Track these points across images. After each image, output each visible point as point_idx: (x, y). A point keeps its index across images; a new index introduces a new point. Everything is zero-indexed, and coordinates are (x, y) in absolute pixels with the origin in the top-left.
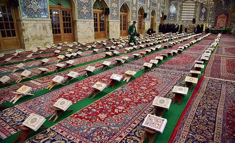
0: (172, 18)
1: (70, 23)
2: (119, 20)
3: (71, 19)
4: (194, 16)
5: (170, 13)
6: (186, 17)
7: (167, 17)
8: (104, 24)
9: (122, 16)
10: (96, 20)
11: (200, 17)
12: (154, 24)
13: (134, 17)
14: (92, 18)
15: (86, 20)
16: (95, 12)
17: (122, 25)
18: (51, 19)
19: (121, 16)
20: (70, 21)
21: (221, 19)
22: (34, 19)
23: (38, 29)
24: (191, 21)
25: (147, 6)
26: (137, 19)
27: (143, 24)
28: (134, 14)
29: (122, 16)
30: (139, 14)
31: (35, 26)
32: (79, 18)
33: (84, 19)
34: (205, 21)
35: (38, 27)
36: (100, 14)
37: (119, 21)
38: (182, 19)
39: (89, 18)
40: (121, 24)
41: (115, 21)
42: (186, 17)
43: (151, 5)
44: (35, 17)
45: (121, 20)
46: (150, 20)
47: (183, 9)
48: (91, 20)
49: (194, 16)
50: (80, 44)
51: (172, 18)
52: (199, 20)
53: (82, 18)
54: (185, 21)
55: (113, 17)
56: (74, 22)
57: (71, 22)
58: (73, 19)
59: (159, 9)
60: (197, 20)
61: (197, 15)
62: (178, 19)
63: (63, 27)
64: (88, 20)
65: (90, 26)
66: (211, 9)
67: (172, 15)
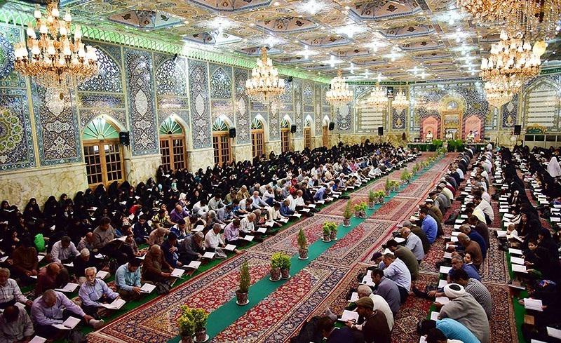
0: (344, 126)
1: (182, 156)
3: (184, 150)
8: (228, 150)
9: (255, 136)
10: (216, 146)
11: (395, 121)
15: (147, 156)
16: (86, 146)
17: (256, 148)
18: (86, 162)
19: (253, 135)
21: (429, 125)
22: (143, 156)
23: (147, 168)
24: (376, 129)
25: (296, 113)
27: (291, 142)
28: (202, 134)
29: (255, 136)
31: (143, 165)
32: (194, 148)
34: (404, 128)
35: (147, 166)
36: (222, 137)
37: (251, 143)
38: (363, 127)
40: (254, 147)
44: (144, 154)
45: (253, 142)
47: (530, 115)
52: (393, 128)
53: (198, 147)
54: (369, 129)
55: (242, 140)
56: (188, 153)
62: (355, 127)
63: (103, 176)
66: (496, 117)
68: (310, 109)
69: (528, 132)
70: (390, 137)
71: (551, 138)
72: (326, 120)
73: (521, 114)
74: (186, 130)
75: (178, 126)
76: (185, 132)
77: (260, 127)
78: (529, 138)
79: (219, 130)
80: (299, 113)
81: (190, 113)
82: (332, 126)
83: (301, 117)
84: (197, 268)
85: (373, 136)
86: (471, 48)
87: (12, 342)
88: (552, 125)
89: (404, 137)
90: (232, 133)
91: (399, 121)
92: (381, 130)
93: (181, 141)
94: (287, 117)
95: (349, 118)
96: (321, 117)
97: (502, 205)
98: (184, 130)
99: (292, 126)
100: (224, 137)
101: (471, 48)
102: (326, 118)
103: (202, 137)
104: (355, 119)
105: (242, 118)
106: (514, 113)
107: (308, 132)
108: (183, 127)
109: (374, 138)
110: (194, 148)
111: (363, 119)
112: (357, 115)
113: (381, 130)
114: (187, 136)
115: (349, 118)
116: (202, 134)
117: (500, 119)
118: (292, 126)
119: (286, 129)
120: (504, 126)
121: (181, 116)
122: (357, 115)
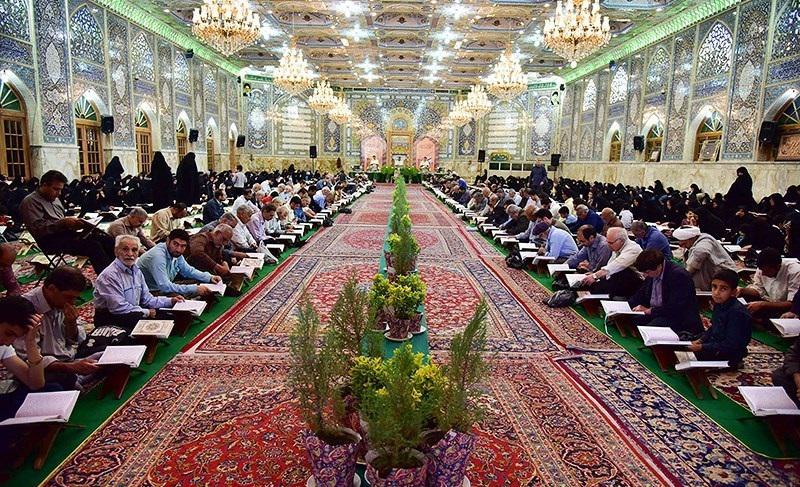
0: (258, 142)
1: (21, 152)
2: (73, 142)
4: (311, 139)
5: (253, 131)
6: (294, 141)
7: (247, 139)
8: (97, 154)
11: (327, 142)
12: (216, 157)
13: (124, 135)
14: (73, 140)
15: (61, 145)
19: (79, 130)
20: (21, 146)
26: (135, 141)
30: (138, 125)
32: (45, 141)
33: (57, 142)
38: (284, 147)
39: (68, 139)
41: (125, 148)
42: (294, 141)
43: (132, 90)
46: (176, 144)
48: (71, 146)
49: (311, 139)
50: (652, 161)
51: (258, 142)
53: (52, 140)
54: (293, 150)
57: (24, 149)
58: (28, 142)
59: (224, 119)
60: (319, 150)
61: (319, 136)
62: (274, 146)
64: (65, 145)
65: (70, 161)
67: (259, 136)
68: (215, 110)
69: (492, 160)
70: (321, 163)
71: (517, 167)
72: (234, 130)
73: (480, 139)
74: (29, 104)
75: (12, 96)
76: (25, 107)
77: (145, 125)
78: (493, 167)
79: (83, 116)
80: (199, 113)
81: (37, 74)
82: (241, 141)
83: (202, 119)
84: (66, 416)
85: (299, 160)
86: (374, 66)
87: (563, 485)
88: (514, 152)
89: (339, 163)
90: (108, 124)
91: (332, 141)
92: (313, 151)
93: (19, 124)
94: (183, 116)
95: (265, 135)
96: (226, 125)
97: (524, 250)
98: (24, 103)
99: (192, 132)
100: (95, 130)
101: (374, 66)
102: (233, 127)
103: (59, 124)
104: (273, 134)
105: (121, 102)
106: (472, 138)
107: (211, 145)
108: (22, 99)
109: (302, 162)
110: (45, 141)
111: (284, 134)
112: (276, 128)
113: (313, 151)
114: (30, 116)
115: (265, 135)
116: (58, 116)
117: (455, 144)
118: (192, 132)
119: (182, 135)
120: (461, 153)
121: (20, 75)
122: (276, 128)
